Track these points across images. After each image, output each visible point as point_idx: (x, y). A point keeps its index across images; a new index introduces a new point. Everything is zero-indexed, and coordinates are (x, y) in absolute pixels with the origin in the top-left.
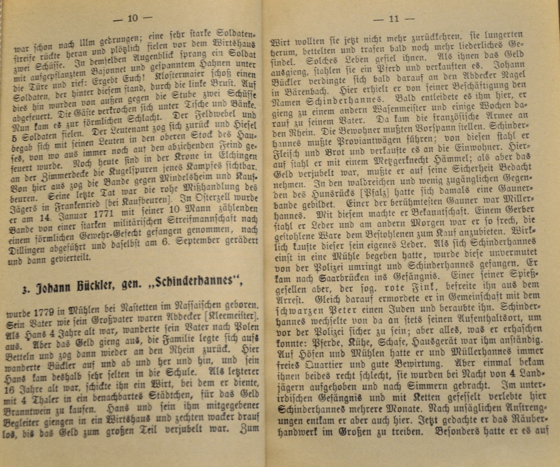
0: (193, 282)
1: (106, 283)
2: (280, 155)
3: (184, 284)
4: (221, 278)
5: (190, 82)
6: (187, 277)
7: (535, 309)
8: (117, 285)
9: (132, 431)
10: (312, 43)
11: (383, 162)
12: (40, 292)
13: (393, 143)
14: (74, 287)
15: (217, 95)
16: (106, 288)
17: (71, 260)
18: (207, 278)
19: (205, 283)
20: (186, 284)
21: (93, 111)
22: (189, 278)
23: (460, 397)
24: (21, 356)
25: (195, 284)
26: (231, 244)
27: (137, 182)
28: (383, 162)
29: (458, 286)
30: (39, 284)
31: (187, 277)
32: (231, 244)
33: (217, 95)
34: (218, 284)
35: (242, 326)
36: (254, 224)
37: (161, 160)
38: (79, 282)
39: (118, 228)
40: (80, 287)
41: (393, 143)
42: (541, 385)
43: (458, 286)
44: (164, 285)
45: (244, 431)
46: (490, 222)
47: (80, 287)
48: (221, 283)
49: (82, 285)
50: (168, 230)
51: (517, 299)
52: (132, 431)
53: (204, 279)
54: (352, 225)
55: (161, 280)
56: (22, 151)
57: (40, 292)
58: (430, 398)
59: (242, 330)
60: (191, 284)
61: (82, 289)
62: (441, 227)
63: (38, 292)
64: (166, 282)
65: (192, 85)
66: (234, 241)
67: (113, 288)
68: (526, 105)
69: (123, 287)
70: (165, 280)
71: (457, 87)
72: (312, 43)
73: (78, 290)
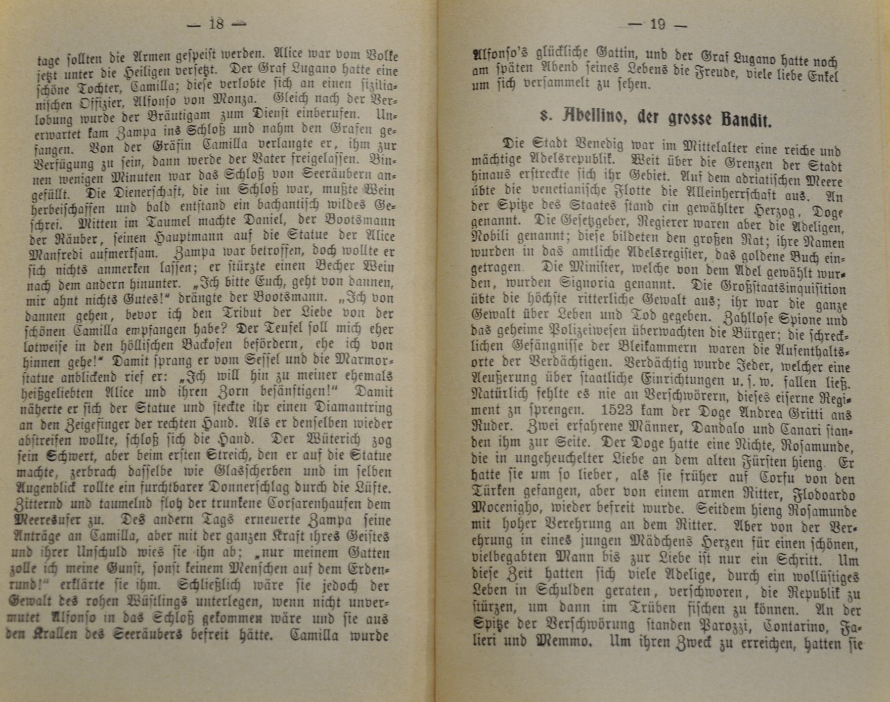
1: (650, 114)
3: (752, 125)
5: (580, 471)
8: (631, 115)
13: (387, 135)
14: (717, 119)
15: (553, 427)
16: (650, 122)
21: (301, 52)
22: (646, 113)
26: (254, 541)
29: (614, 508)
32: (254, 541)
33: (553, 427)
35: (560, 329)
36: (355, 335)
37: (677, 629)
38: (723, 113)
40: (727, 120)
41: (387, 135)
42: (392, 102)
43: (614, 508)
45: (681, 646)
46: (566, 475)
47: (727, 120)
48: (613, 120)
49: (729, 118)
50: (88, 162)
51: (511, 319)
54: (296, 283)
58: (581, 443)
59: (560, 334)
61: (729, 124)
62: (321, 398)
65: (583, 476)
66: (618, 592)
67: (625, 121)
68: (395, 87)
69: (671, 121)
73: (724, 124)
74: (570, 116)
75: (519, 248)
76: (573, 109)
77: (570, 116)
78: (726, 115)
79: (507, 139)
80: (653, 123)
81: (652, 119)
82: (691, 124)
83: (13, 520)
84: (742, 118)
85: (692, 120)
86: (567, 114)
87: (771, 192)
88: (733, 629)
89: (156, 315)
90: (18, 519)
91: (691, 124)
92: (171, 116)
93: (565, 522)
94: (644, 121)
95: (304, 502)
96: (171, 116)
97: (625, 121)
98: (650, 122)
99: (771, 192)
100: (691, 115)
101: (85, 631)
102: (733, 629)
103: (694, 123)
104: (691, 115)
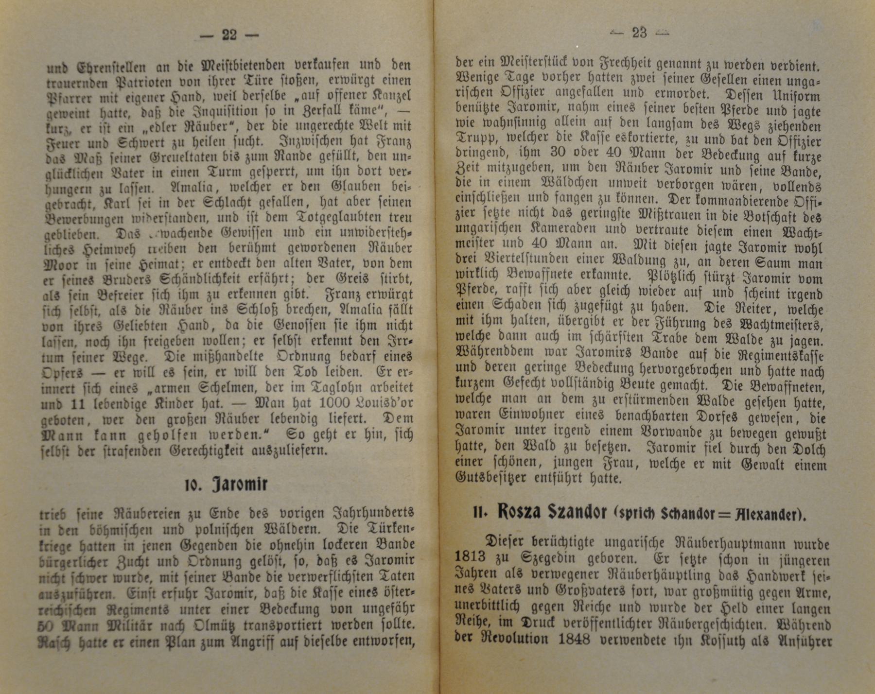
0: (791, 517)
2: (665, 324)
3: (587, 516)
4: (581, 509)
6: (590, 505)
7: (407, 595)
9: (545, 640)
10: (401, 625)
11: (215, 67)
12: (218, 489)
14: (545, 512)
17: (68, 393)
18: (685, 511)
19: (683, 517)
20: (782, 518)
22: (703, 511)
23: (598, 623)
24: (100, 641)
25: (794, 519)
27: (322, 158)
28: (215, 67)
30: (216, 477)
31: (590, 505)
34: (577, 517)
39: (508, 405)
44: (671, 517)
48: (582, 517)
52: (545, 640)
53: (681, 513)
55: (668, 512)
56: (757, 360)
57: (218, 489)
60: (789, 519)
63: (216, 489)
64: (673, 514)
70: (672, 511)
71: (708, 156)
72: (401, 625)
74: (741, 516)
75: (207, 307)
76: (743, 510)
77: (741, 516)
78: (503, 506)
79: (491, 535)
80: (791, 520)
81: (791, 517)
82: (516, 517)
83: (41, 437)
84: (577, 509)
85: (517, 513)
86: (739, 514)
87: (792, 214)
88: (273, 453)
89: (77, 266)
90: (45, 436)
91: (516, 517)
92: (132, 515)
93: (189, 449)
94: (591, 517)
95: (474, 412)
96: (132, 515)
97: (805, 519)
98: (789, 519)
99: (792, 214)
100: (516, 508)
101: (77, 449)
102: (273, 453)
103: (520, 516)
104: (516, 508)
